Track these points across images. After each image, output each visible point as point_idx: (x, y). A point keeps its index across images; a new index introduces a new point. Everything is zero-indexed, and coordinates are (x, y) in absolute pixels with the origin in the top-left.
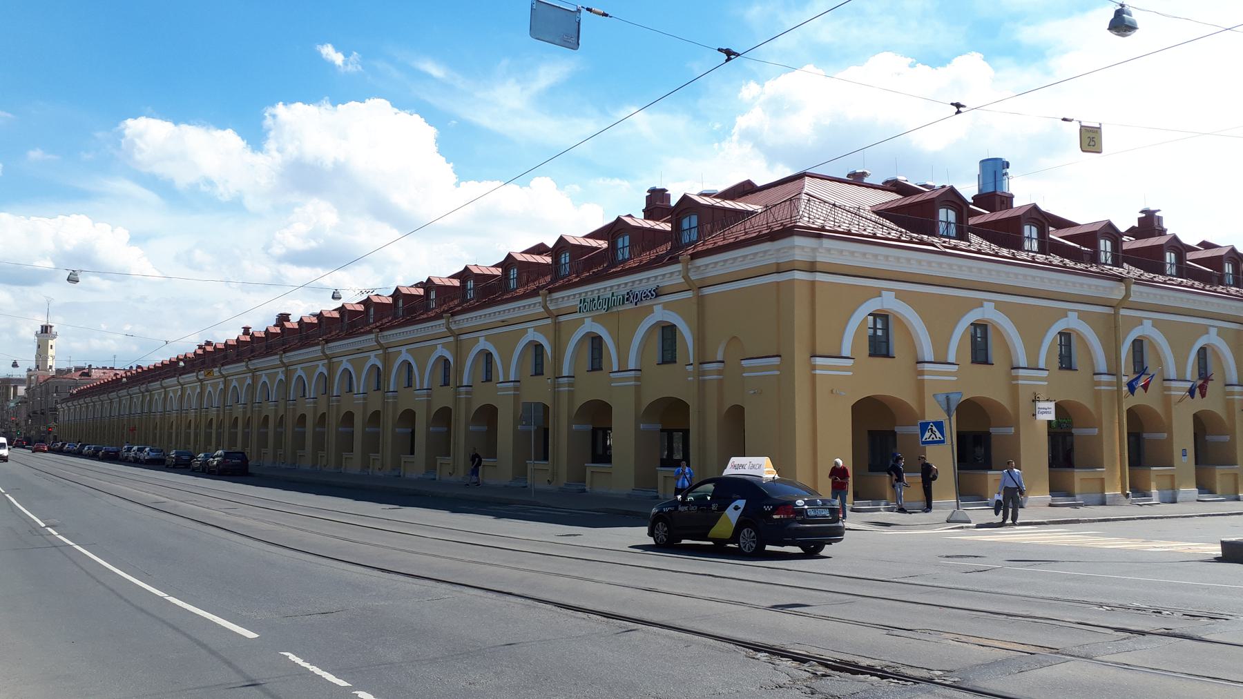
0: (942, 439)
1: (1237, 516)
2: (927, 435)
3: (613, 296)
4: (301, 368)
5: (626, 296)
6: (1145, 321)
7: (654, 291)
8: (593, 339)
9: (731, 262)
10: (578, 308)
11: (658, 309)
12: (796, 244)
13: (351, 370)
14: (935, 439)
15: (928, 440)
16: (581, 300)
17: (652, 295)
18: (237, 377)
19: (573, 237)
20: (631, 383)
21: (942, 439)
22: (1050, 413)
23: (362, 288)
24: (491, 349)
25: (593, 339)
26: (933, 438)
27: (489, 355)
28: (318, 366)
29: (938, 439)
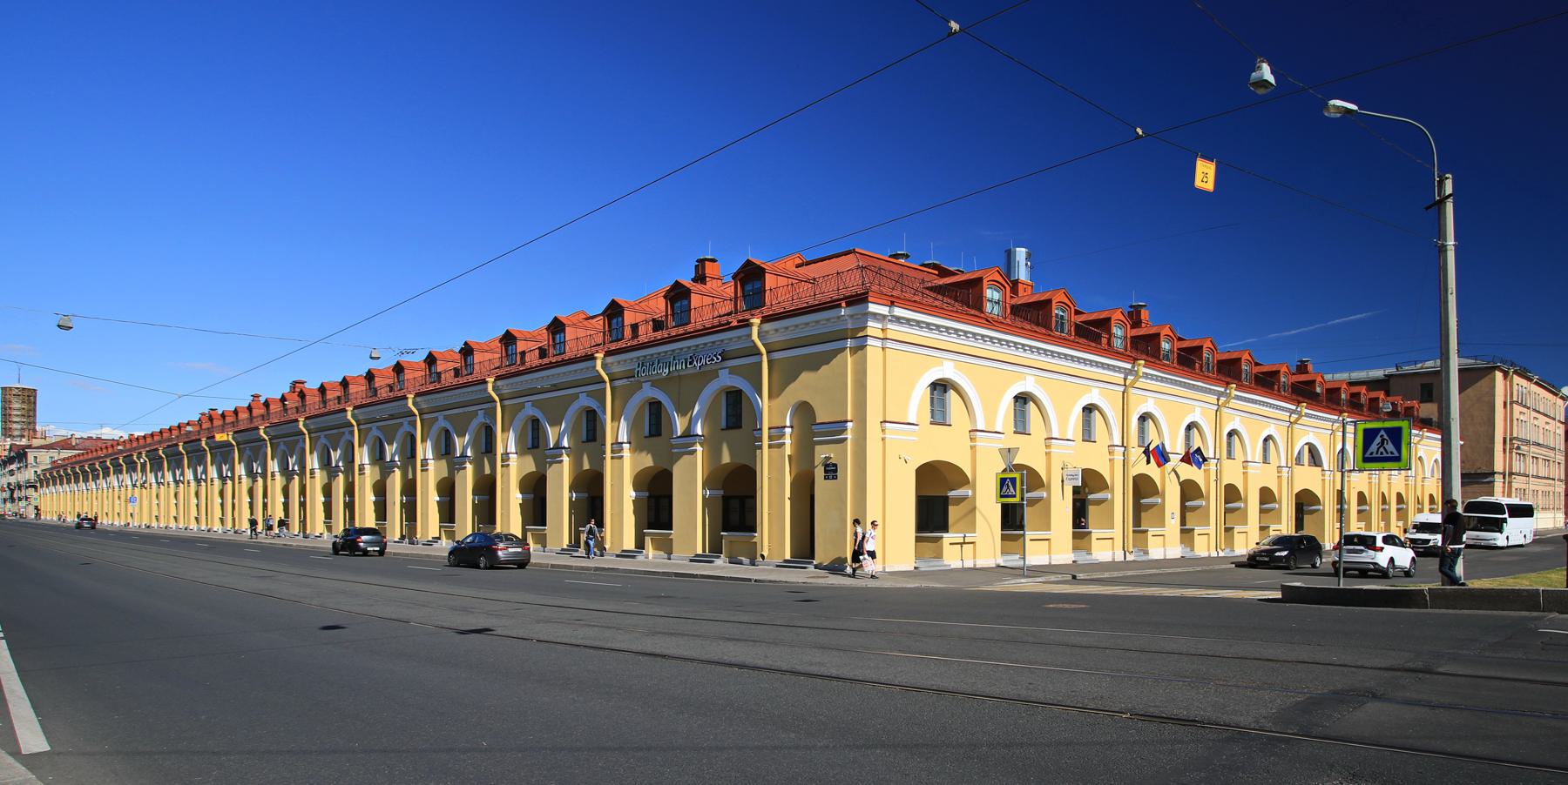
0: (1396, 454)
1: (478, 635)
2: (1005, 488)
3: (674, 359)
4: (325, 436)
5: (689, 360)
6: (1149, 399)
7: (720, 355)
8: (533, 421)
9: (814, 324)
10: (636, 372)
11: (724, 374)
12: (870, 310)
13: (381, 437)
14: (1385, 455)
15: (1374, 455)
16: (639, 364)
17: (718, 359)
18: (285, 439)
19: (519, 331)
20: (676, 450)
21: (1396, 454)
22: (1077, 479)
23: (402, 348)
24: (539, 415)
25: (533, 421)
26: (1382, 453)
27: (447, 431)
28: (344, 433)
29: (1390, 455)
